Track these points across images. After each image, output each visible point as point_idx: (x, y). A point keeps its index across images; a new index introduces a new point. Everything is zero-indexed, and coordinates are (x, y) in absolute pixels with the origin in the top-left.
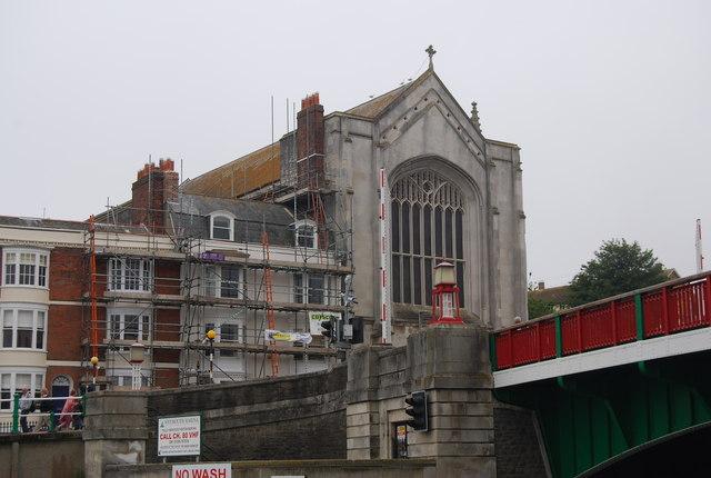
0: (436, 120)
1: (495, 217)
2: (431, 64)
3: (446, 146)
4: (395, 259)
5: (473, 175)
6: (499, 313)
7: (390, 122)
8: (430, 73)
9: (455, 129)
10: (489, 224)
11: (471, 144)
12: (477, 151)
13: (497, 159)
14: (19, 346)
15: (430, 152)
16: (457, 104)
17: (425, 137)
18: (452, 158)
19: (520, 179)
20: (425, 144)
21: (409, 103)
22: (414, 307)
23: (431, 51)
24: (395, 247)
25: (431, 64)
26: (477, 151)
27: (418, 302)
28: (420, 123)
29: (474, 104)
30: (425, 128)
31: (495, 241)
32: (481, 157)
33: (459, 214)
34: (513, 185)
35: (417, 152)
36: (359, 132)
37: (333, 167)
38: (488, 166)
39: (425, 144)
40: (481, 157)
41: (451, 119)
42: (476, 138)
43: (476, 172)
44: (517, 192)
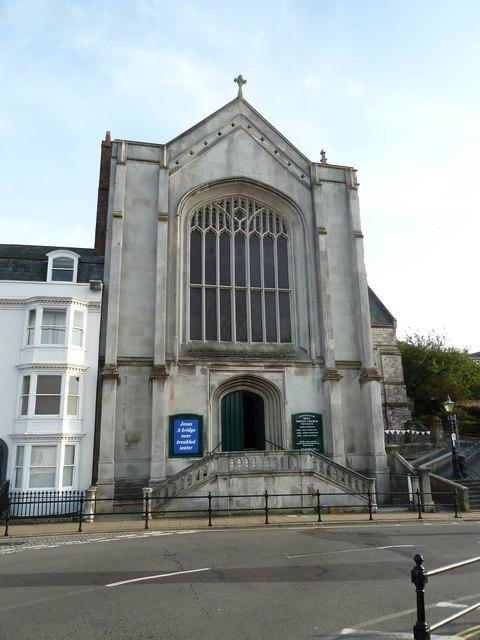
0: (245, 144)
1: (322, 238)
2: (240, 92)
3: (263, 171)
4: (196, 293)
5: (294, 196)
6: (331, 344)
7: (184, 146)
8: (239, 99)
9: (297, 178)
10: (316, 245)
11: (292, 168)
12: (299, 174)
13: (323, 181)
14: (37, 413)
15: (235, 174)
16: (265, 122)
17: (228, 160)
18: (266, 179)
19: (356, 198)
20: (229, 166)
21: (209, 127)
22: (220, 345)
23: (240, 81)
24: (195, 276)
25: (240, 92)
26: (299, 174)
27: (227, 337)
28: (223, 145)
29: (323, 153)
30: (229, 151)
31: (322, 263)
32: (306, 179)
33: (283, 241)
34: (348, 206)
35: (219, 175)
36: (143, 158)
37: (327, 293)
38: (312, 187)
39: (229, 166)
40: (306, 179)
41: (266, 143)
42: (298, 160)
43: (296, 192)
44: (353, 212)
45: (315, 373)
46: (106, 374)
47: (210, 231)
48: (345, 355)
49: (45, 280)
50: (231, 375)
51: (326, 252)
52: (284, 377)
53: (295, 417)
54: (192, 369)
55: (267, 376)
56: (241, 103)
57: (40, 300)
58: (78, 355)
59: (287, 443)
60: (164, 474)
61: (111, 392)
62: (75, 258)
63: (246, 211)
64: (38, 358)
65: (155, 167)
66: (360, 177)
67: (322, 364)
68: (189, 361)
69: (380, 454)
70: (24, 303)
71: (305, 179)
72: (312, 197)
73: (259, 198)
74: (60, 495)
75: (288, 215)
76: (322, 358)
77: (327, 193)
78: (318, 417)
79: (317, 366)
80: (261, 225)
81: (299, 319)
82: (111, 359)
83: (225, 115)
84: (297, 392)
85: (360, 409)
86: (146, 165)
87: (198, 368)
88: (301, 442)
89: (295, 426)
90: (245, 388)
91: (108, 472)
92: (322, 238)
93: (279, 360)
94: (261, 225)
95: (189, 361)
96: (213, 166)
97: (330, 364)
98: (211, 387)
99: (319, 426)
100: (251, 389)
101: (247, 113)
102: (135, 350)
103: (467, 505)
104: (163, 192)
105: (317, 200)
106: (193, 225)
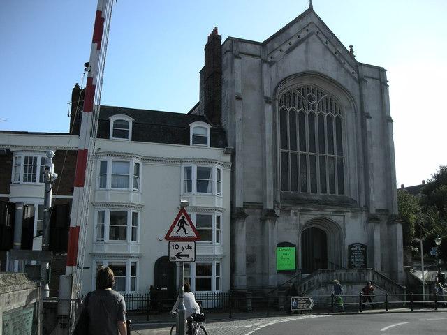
0: (316, 46)
1: (368, 121)
3: (328, 67)
5: (349, 88)
6: (373, 198)
10: (364, 126)
11: (346, 65)
21: (292, 31)
28: (303, 46)
30: (306, 52)
33: (339, 120)
35: (301, 69)
45: (363, 217)
46: (237, 214)
47: (310, 113)
48: (380, 205)
49: (109, 138)
50: (313, 217)
51: (371, 132)
52: (344, 219)
53: (350, 246)
54: (289, 212)
55: (334, 218)
56: (312, 14)
57: (194, 160)
58: (218, 201)
59: (345, 264)
60: (276, 284)
61: (242, 228)
62: (130, 120)
63: (315, 96)
64: (109, 198)
65: (257, 60)
66: (389, 76)
67: (368, 211)
68: (286, 207)
69: (401, 272)
70: (181, 161)
71: (354, 75)
72: (361, 90)
73: (324, 87)
74: (134, 296)
75: (343, 100)
76: (367, 206)
77: (370, 87)
78: (364, 246)
79: (364, 212)
80: (325, 107)
81: (351, 180)
82: (239, 204)
83: (302, 23)
84: (353, 230)
85: (389, 242)
86: (251, 58)
87: (292, 212)
88: (354, 264)
89: (351, 253)
90: (316, 226)
91: (242, 281)
92: (368, 121)
93: (344, 204)
94: (325, 107)
95: (286, 207)
96: (295, 62)
97: (373, 211)
98: (301, 225)
99: (364, 253)
100: (319, 227)
101: (316, 21)
102: (253, 198)
103: (249, 305)
104: (266, 81)
105: (365, 92)
106: (281, 105)
